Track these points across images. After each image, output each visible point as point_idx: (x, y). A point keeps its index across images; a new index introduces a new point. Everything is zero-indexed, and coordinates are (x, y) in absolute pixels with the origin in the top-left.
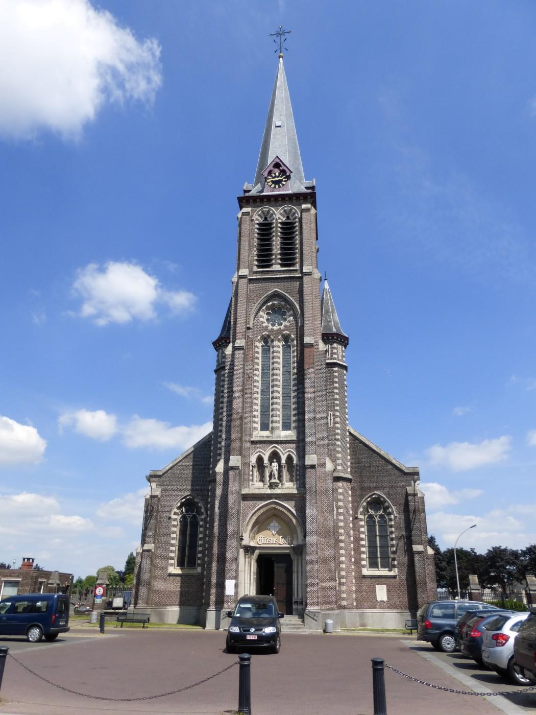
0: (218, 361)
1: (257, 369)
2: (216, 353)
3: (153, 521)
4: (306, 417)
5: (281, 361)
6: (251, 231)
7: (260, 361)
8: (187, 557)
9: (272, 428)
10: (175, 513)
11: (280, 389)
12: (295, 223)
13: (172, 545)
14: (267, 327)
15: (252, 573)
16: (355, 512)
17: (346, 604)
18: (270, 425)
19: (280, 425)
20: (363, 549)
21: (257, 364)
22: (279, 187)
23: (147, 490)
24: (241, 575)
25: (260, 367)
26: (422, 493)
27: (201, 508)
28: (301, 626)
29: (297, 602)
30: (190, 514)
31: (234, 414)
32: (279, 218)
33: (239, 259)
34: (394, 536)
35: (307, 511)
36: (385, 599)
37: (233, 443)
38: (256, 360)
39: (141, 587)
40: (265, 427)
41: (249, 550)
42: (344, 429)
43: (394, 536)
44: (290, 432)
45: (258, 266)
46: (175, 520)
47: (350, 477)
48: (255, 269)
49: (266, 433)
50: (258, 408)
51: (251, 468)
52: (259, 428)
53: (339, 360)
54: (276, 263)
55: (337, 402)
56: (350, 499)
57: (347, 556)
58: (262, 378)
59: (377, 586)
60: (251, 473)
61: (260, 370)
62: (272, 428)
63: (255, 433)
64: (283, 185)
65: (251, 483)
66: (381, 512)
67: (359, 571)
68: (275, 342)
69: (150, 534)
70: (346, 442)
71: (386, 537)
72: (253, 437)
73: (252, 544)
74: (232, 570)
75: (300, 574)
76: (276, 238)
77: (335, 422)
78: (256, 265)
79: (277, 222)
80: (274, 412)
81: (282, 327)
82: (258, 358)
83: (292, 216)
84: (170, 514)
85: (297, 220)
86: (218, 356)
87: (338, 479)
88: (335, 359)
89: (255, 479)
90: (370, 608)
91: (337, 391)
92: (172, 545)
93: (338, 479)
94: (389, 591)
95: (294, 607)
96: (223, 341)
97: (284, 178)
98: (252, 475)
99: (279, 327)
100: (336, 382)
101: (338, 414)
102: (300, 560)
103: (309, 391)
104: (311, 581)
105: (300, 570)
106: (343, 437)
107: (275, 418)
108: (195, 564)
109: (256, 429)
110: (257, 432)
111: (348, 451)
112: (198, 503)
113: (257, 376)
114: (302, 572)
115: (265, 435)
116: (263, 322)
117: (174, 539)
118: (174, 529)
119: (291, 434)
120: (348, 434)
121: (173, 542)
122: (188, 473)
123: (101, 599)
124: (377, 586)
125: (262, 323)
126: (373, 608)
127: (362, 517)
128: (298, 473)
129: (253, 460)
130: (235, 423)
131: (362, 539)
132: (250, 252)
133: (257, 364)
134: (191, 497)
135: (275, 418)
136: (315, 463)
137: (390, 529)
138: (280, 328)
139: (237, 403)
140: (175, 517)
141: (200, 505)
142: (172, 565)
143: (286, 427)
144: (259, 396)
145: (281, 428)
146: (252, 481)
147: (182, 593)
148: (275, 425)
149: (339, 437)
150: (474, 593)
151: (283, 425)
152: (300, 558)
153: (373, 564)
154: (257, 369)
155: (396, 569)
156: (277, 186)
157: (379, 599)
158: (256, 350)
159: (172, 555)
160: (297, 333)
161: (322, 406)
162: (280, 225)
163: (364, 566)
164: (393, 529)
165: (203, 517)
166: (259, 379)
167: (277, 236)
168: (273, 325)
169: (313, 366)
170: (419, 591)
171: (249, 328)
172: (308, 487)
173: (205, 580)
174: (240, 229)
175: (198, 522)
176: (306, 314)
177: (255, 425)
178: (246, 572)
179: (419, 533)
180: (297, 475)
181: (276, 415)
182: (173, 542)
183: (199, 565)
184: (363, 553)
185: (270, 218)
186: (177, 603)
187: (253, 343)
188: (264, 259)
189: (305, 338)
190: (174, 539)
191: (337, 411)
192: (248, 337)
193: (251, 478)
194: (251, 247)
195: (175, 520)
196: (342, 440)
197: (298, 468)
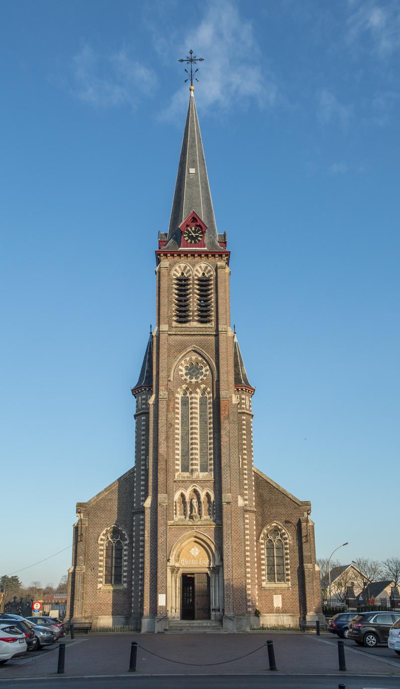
0: (137, 406)
1: (177, 418)
2: (135, 400)
3: (81, 545)
4: (223, 462)
5: (198, 411)
6: (169, 288)
7: (179, 411)
8: (114, 576)
9: (192, 471)
10: (102, 540)
11: (198, 436)
12: (211, 280)
13: (100, 566)
14: (186, 380)
15: (177, 588)
16: (258, 538)
17: (251, 610)
18: (190, 467)
19: (198, 467)
20: (263, 567)
21: (178, 413)
22: (195, 242)
23: (75, 519)
24: (169, 590)
25: (179, 416)
26: (312, 522)
27: (124, 535)
28: (219, 628)
29: (214, 610)
30: (114, 540)
31: (160, 458)
32: (196, 275)
33: (159, 314)
34: (288, 556)
35: (225, 539)
36: (280, 605)
37: (160, 484)
38: (176, 410)
39: (75, 601)
40: (185, 468)
41: (174, 570)
42: (250, 470)
43: (288, 556)
44: (207, 473)
45: (177, 321)
46: (102, 545)
47: (255, 510)
48: (174, 324)
49: (186, 474)
50: (179, 452)
51: (174, 504)
52: (180, 470)
53: (246, 410)
54: (193, 320)
55: (245, 447)
56: (255, 528)
57: (252, 573)
58: (182, 426)
59: (274, 596)
60: (175, 508)
61: (180, 419)
62: (192, 471)
63: (177, 474)
64: (199, 241)
65: (175, 516)
66: (279, 538)
67: (260, 585)
68: (193, 394)
69: (81, 557)
70: (252, 480)
71: (282, 557)
72: (176, 477)
73: (177, 565)
74: (163, 586)
75: (217, 588)
76: (193, 294)
77: (243, 464)
78: (175, 321)
79: (194, 279)
80: (193, 457)
81: (199, 380)
82: (178, 408)
83: (207, 273)
84: (97, 540)
85: (212, 278)
86: (137, 402)
87: (246, 511)
88: (243, 409)
89: (178, 513)
90: (268, 613)
91: (244, 437)
92: (100, 566)
93: (246, 511)
94: (283, 599)
95: (213, 613)
96: (143, 389)
97: (200, 234)
98: (176, 510)
99: (196, 380)
100: (244, 430)
101: (246, 457)
102: (217, 578)
103: (224, 439)
104: (228, 594)
105: (217, 585)
106: (249, 475)
107: (194, 462)
108: (121, 581)
109: (178, 470)
110: (179, 473)
111: (254, 488)
112: (121, 531)
113: (178, 424)
114: (219, 586)
115: (186, 476)
116: (182, 376)
117: (101, 561)
118: (101, 553)
119: (209, 476)
120: (253, 473)
121: (101, 563)
122: (114, 506)
123: (39, 613)
124: (274, 596)
125: (182, 376)
126: (271, 613)
127: (263, 541)
128: (215, 508)
129: (177, 496)
130: (161, 465)
131: (263, 559)
132: (170, 308)
133: (178, 413)
134: (115, 526)
135: (194, 462)
136: (231, 500)
137: (286, 551)
138: (198, 382)
139: (162, 449)
140: (102, 542)
141: (123, 532)
142: (101, 582)
143: (204, 469)
144: (179, 442)
145: (199, 470)
146: (176, 514)
147: (114, 605)
148: (194, 467)
149: (246, 477)
150: (350, 600)
151: (200, 468)
152: (217, 576)
153: (271, 579)
154: (177, 418)
155: (290, 582)
156: (193, 242)
157: (275, 605)
158: (176, 400)
159: (101, 574)
160: (213, 387)
161: (235, 450)
162: (197, 282)
163: (263, 581)
164: (288, 551)
165: (127, 542)
166: (179, 427)
167: (194, 293)
168: (191, 378)
169: (228, 417)
170: (308, 599)
171: (169, 381)
172: (224, 520)
173: (133, 594)
174: (159, 284)
175: (122, 546)
176: (222, 371)
177: (177, 467)
178: (173, 588)
179: (309, 554)
180: (214, 510)
181: (196, 459)
182: (101, 563)
183: (125, 582)
184: (263, 570)
185: (186, 274)
186: (110, 613)
187: (173, 395)
188: (183, 316)
189: (221, 392)
190: (101, 561)
191: (245, 454)
192: (170, 389)
193: (175, 512)
194: (170, 302)
195: (102, 545)
196: (249, 479)
197: (215, 504)
